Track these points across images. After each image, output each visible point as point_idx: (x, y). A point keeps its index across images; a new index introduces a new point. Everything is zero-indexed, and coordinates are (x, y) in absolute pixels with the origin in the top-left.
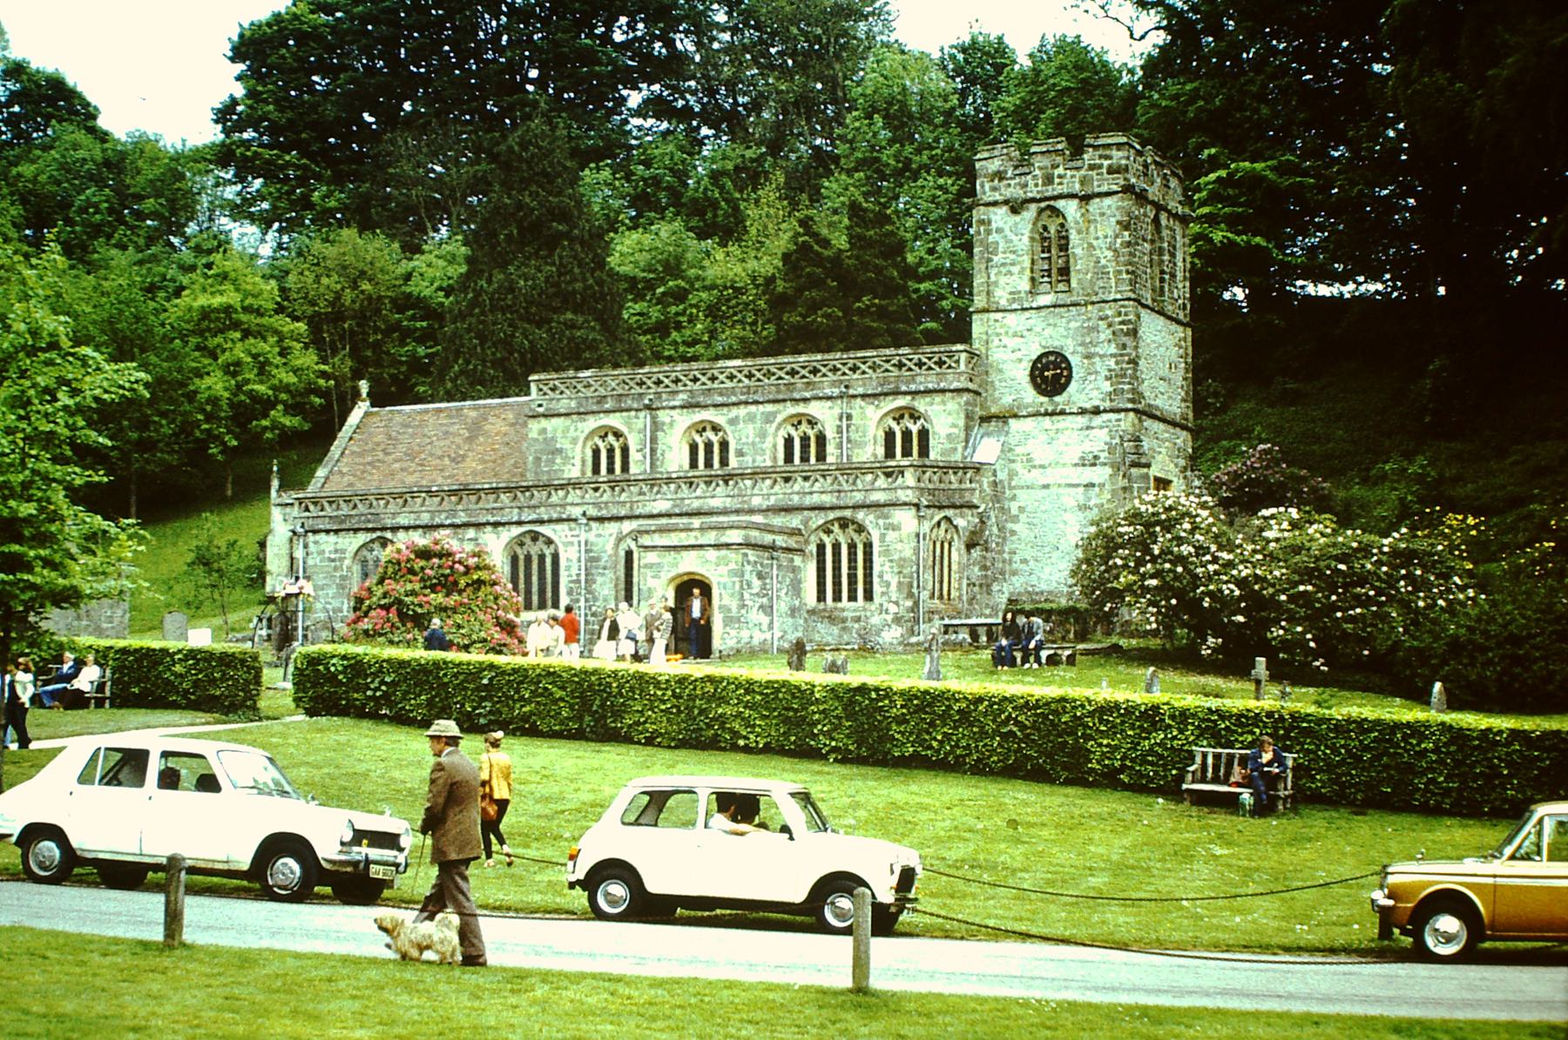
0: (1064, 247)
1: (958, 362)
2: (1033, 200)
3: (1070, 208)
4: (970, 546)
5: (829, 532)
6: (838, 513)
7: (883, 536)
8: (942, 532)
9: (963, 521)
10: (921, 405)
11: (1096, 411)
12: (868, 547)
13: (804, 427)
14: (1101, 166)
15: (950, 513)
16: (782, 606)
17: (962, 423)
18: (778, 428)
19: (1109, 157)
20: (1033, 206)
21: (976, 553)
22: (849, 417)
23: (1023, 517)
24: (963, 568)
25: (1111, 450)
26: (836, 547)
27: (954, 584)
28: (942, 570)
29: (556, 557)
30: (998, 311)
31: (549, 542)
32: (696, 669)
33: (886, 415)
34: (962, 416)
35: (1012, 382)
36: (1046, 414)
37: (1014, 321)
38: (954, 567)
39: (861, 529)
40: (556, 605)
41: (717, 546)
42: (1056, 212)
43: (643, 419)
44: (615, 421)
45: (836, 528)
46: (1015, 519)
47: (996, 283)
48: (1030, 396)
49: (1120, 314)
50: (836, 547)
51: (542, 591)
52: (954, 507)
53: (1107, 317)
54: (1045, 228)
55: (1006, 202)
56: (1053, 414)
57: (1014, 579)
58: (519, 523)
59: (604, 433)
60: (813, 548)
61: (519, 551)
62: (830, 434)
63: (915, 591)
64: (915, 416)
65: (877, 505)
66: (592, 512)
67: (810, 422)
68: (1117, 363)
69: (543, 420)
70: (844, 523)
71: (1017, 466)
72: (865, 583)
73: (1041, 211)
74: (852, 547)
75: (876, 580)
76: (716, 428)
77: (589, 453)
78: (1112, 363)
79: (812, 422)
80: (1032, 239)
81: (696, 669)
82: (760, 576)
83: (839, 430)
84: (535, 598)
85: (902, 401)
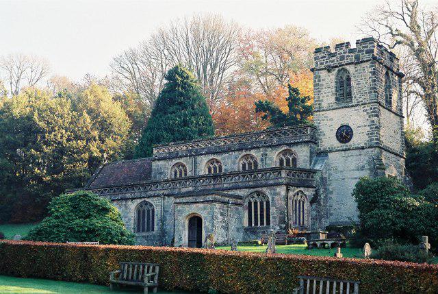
0: (349, 85)
1: (307, 131)
2: (336, 67)
3: (351, 69)
4: (312, 202)
5: (253, 197)
6: (256, 189)
7: (273, 199)
8: (299, 198)
9: (309, 193)
10: (294, 149)
11: (363, 148)
12: (268, 203)
13: (288, 156)
14: (363, 51)
15: (302, 189)
16: (232, 227)
17: (309, 155)
18: (240, 160)
19: (367, 47)
20: (337, 69)
21: (314, 205)
22: (266, 155)
23: (334, 192)
24: (309, 212)
25: (369, 163)
26: (256, 203)
27: (305, 219)
28: (300, 212)
29: (153, 211)
30: (323, 111)
31: (151, 205)
32: (196, 250)
33: (280, 153)
34: (309, 152)
36: (343, 150)
37: (330, 114)
38: (305, 212)
39: (264, 195)
40: (153, 230)
41: (202, 202)
42: (345, 70)
43: (190, 160)
45: (255, 196)
46: (331, 193)
47: (322, 100)
49: (371, 109)
50: (256, 203)
51: (148, 224)
52: (304, 187)
53: (366, 110)
54: (341, 77)
55: (325, 69)
56: (346, 150)
57: (331, 217)
58: (140, 198)
59: (178, 165)
60: (246, 204)
61: (141, 209)
62: (259, 162)
63: (286, 220)
65: (272, 185)
66: (166, 192)
67: (251, 157)
68: (371, 129)
69: (157, 162)
70: (259, 194)
71: (332, 172)
72: (267, 217)
73: (339, 71)
74: (262, 203)
75: (271, 217)
76: (218, 162)
77: (173, 173)
78: (368, 128)
79: (252, 158)
80: (336, 82)
81: (196, 250)
82: (222, 214)
83: (262, 160)
84: (141, 228)
85: (285, 148)
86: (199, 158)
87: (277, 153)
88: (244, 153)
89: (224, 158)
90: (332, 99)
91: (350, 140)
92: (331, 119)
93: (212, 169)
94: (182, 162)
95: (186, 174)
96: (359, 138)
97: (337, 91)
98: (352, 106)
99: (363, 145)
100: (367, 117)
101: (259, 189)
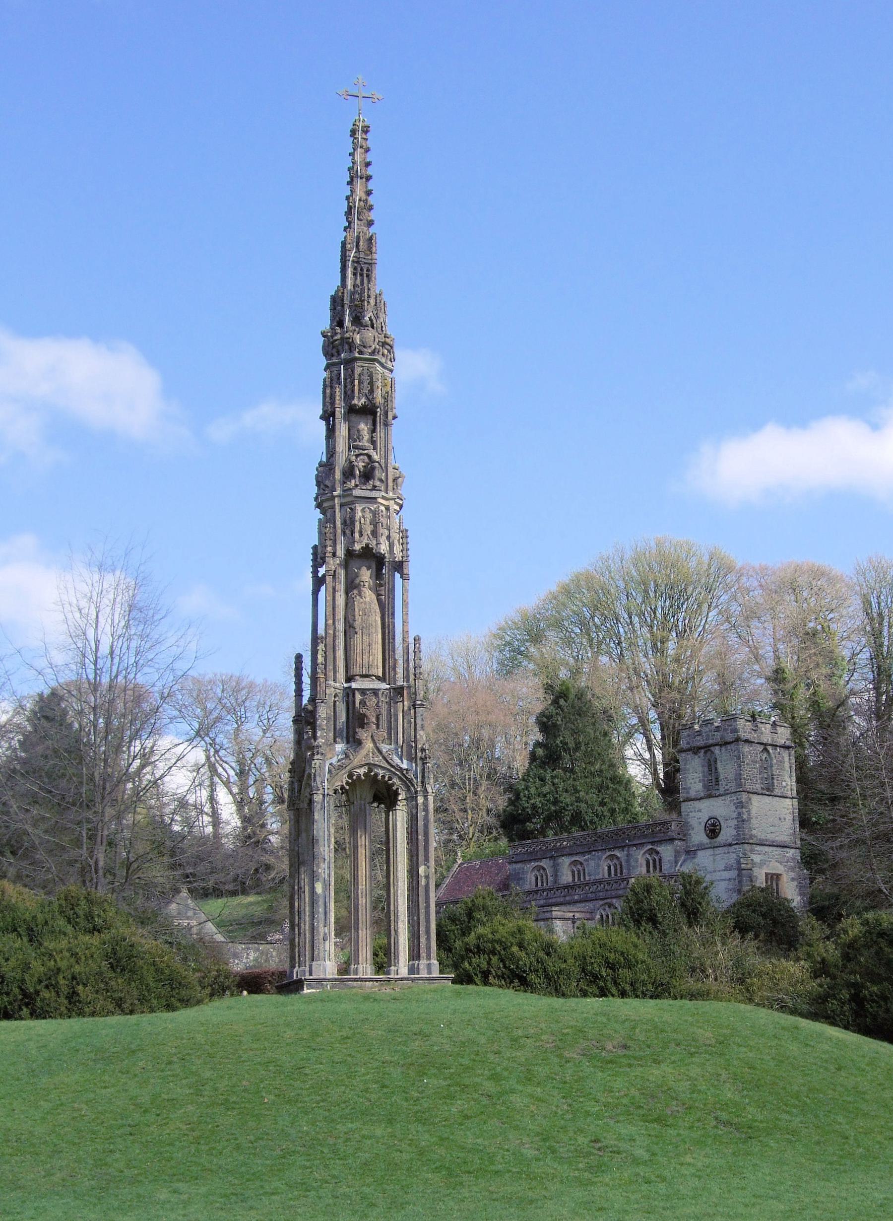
5: (604, 910)
6: (606, 901)
11: (730, 845)
35: (698, 836)
44: (618, 853)
48: (705, 840)
64: (657, 853)
76: (581, 864)
85: (650, 847)
86: (560, 860)
87: (642, 852)
88: (608, 853)
89: (587, 860)
90: (700, 786)
91: (716, 837)
92: (700, 811)
93: (651, 862)
94: (541, 864)
95: (621, 874)
96: (727, 834)
97: (704, 776)
98: (719, 795)
99: (730, 840)
100: (733, 808)
101: (609, 901)
